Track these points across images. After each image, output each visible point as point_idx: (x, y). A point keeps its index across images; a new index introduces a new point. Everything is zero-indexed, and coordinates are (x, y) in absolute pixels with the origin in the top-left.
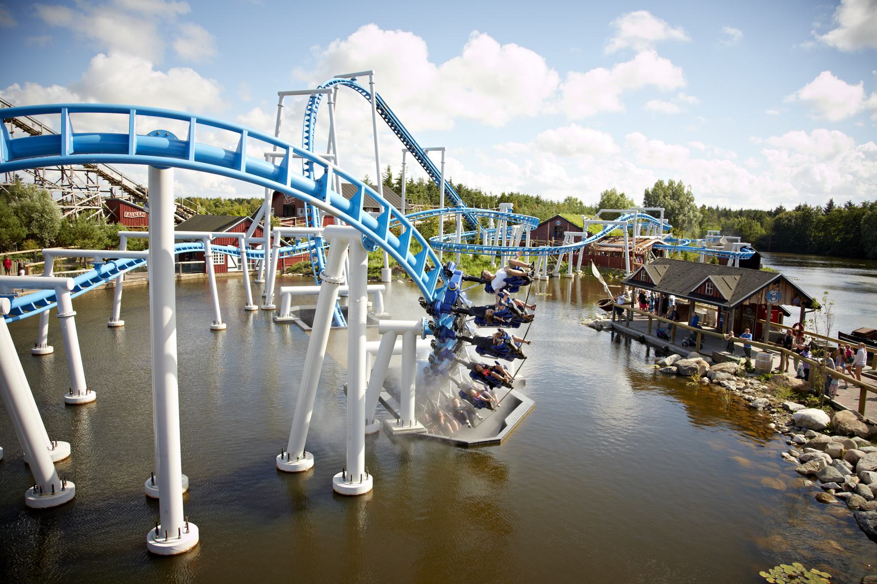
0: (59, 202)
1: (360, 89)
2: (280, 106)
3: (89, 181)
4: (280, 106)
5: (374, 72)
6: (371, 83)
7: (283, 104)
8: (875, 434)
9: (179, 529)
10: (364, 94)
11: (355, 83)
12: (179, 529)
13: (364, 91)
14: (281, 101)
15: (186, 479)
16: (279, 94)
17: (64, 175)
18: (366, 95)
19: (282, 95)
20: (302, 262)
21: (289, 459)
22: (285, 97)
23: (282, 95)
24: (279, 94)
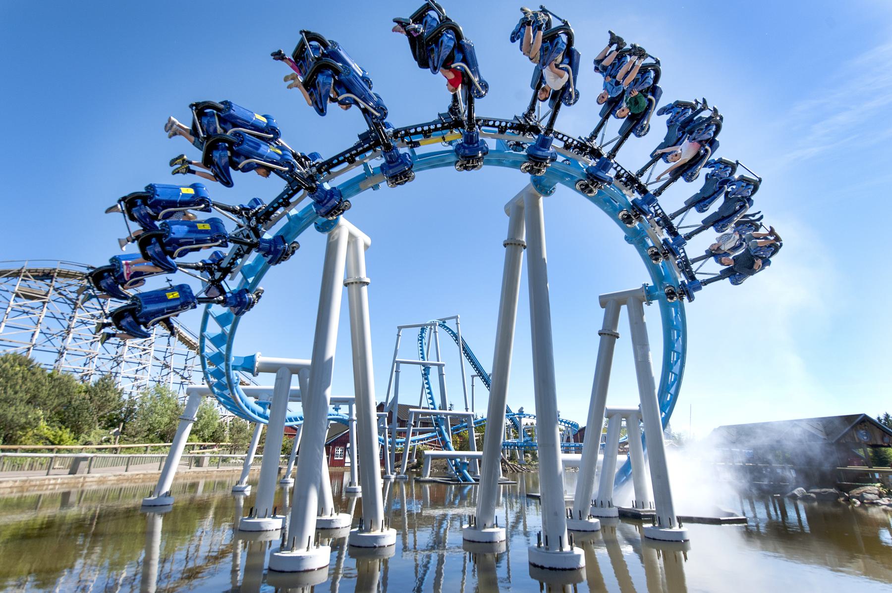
0: (56, 362)
1: (448, 328)
2: (398, 335)
3: (52, 316)
4: (398, 335)
5: (459, 316)
6: (457, 324)
7: (400, 334)
8: (889, 547)
9: (310, 537)
10: (450, 332)
11: (446, 324)
12: (310, 537)
13: (450, 330)
14: (399, 332)
15: (543, 257)
16: (398, 327)
17: (21, 313)
18: (562, 138)
19: (400, 328)
20: (38, 483)
21: (353, 546)
22: (402, 329)
23: (400, 328)
24: (398, 327)
